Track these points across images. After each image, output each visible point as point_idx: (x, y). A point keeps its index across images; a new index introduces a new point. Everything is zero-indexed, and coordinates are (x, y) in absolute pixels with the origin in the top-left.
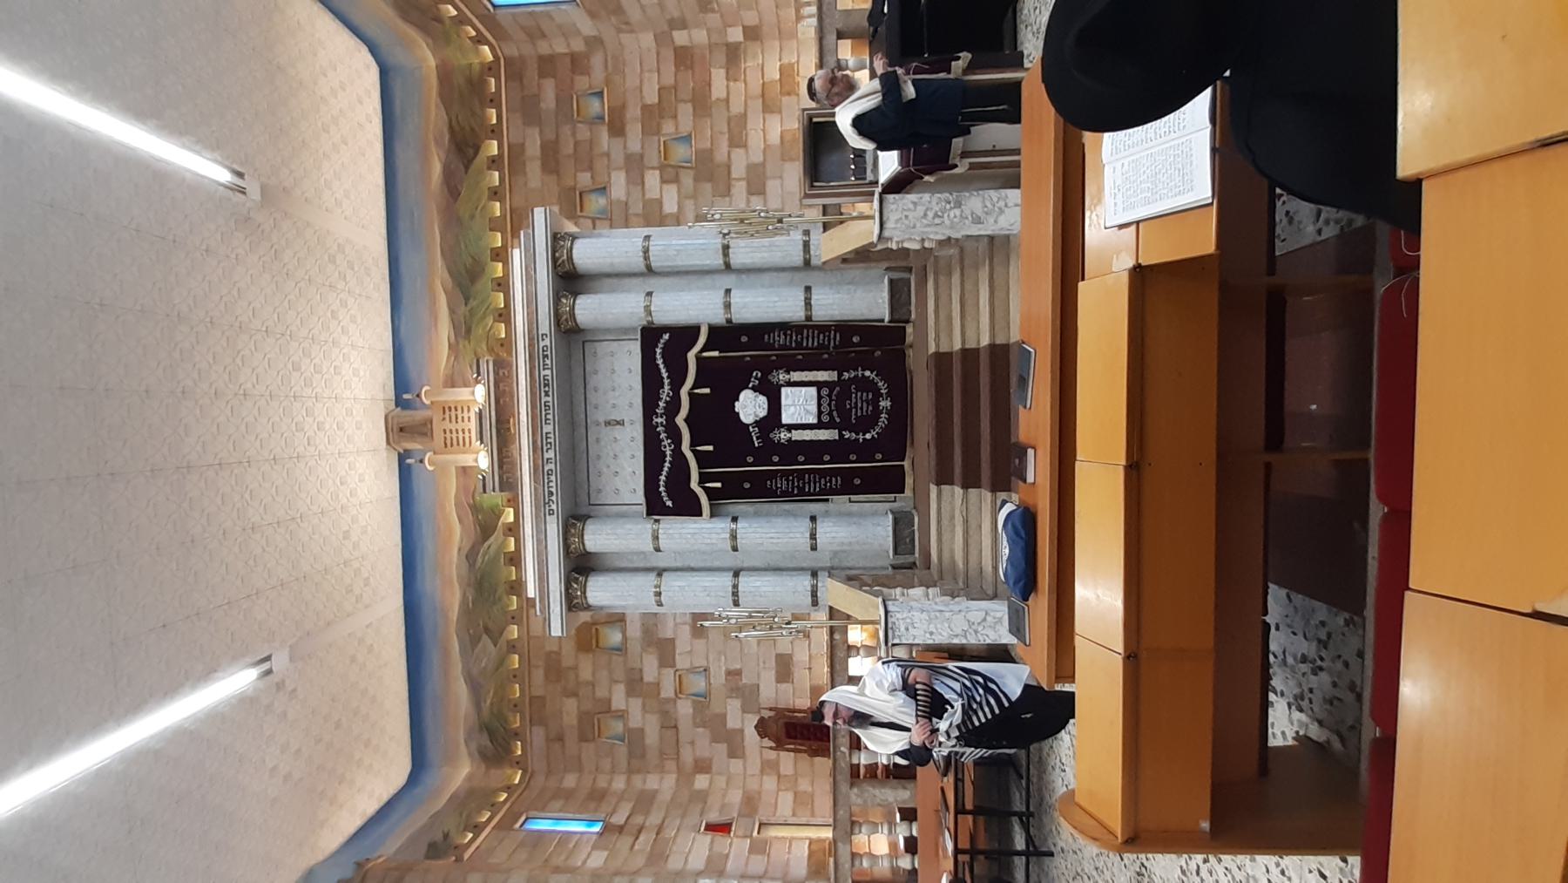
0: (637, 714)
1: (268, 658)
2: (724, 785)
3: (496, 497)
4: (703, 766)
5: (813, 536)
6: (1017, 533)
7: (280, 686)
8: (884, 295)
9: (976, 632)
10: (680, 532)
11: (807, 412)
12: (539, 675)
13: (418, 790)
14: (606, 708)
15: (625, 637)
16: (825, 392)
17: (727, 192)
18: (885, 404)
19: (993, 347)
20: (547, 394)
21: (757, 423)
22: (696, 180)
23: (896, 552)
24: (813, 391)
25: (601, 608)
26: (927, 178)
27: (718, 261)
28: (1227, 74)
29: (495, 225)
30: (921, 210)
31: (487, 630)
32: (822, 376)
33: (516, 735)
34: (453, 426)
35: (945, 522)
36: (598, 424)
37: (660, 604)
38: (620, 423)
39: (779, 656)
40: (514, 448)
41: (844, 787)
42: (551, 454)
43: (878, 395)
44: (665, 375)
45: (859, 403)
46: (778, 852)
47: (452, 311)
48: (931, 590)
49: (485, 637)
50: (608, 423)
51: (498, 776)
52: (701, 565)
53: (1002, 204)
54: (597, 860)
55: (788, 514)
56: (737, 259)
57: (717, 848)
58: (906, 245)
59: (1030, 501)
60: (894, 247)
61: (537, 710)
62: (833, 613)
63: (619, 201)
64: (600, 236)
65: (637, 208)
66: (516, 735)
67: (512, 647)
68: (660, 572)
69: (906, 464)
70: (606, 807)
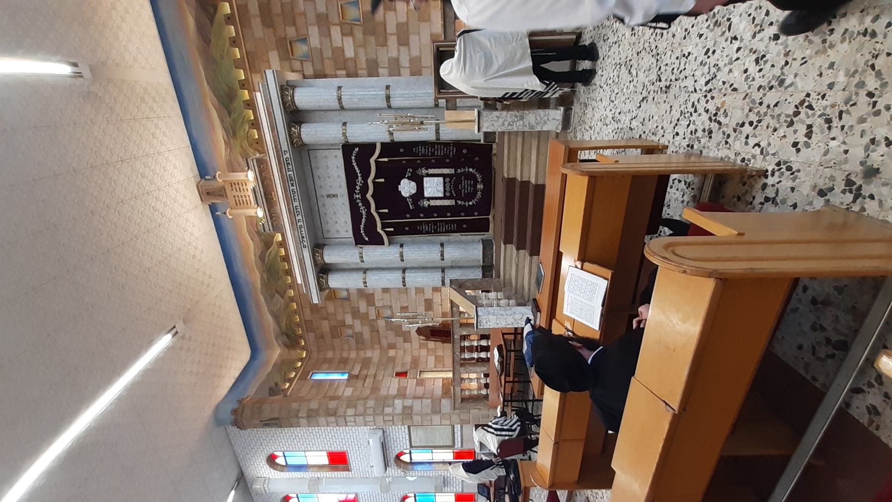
0: (358, 326)
1: (174, 327)
2: (402, 353)
4: (392, 346)
5: (442, 255)
7: (183, 337)
10: (373, 254)
11: (438, 191)
12: (307, 312)
13: (256, 362)
14: (343, 324)
16: (448, 180)
17: (385, 44)
18: (480, 186)
20: (292, 185)
21: (411, 197)
22: (364, 34)
24: (441, 179)
28: (610, 432)
29: (238, 64)
30: (501, 120)
31: (277, 291)
32: (446, 171)
33: (301, 337)
34: (238, 194)
35: (507, 261)
36: (323, 196)
38: (335, 196)
39: (426, 300)
41: (458, 367)
42: (300, 217)
43: (476, 182)
46: (429, 385)
47: (222, 121)
50: (328, 196)
51: (294, 354)
53: (546, 118)
54: (349, 392)
57: (401, 385)
61: (309, 326)
66: (301, 337)
67: (292, 299)
68: (365, 271)
69: (490, 217)
70: (349, 367)
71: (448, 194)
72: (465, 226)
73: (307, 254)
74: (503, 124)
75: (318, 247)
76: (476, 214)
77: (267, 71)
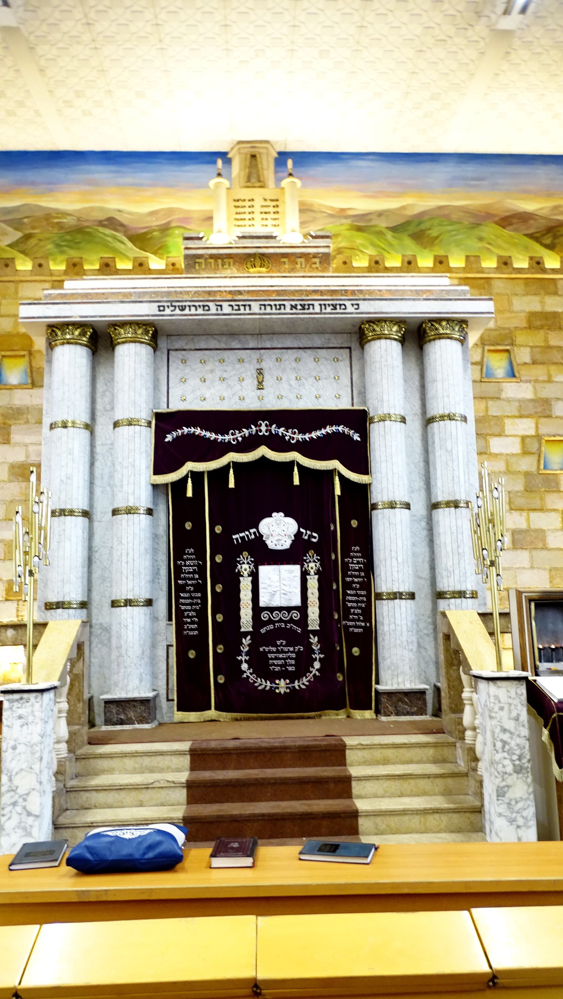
3: (177, 250)
5: (128, 603)
6: (151, 847)
8: (408, 683)
9: (14, 804)
10: (139, 446)
11: (273, 595)
15: (12, 388)
16: (296, 615)
18: (282, 686)
19: (354, 815)
21: (260, 538)
22: (527, 474)
23: (108, 702)
24: (297, 601)
25: (50, 361)
26: (546, 732)
27: (440, 496)
29: (472, 261)
30: (510, 725)
31: (28, 237)
32: (314, 612)
34: (257, 209)
35: (147, 761)
36: (260, 361)
37: (52, 426)
38: (260, 386)
40: (233, 271)
43: (292, 677)
44: (314, 435)
45: (282, 655)
47: (380, 214)
48: (64, 747)
49: (19, 235)
50: (260, 372)
52: (98, 472)
53: (520, 821)
55: (156, 574)
56: (443, 516)
58: (468, 710)
59: (187, 863)
60: (465, 695)
62: (40, 626)
63: (501, 390)
64: (465, 369)
65: (494, 409)
68: (90, 427)
69: (212, 713)
71: (265, 616)
72: (192, 654)
73: (145, 310)
74: (504, 730)
75: (155, 335)
76: (221, 680)
77: (491, 303)
